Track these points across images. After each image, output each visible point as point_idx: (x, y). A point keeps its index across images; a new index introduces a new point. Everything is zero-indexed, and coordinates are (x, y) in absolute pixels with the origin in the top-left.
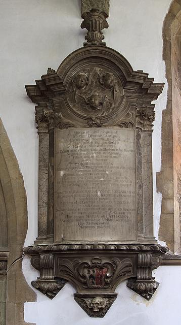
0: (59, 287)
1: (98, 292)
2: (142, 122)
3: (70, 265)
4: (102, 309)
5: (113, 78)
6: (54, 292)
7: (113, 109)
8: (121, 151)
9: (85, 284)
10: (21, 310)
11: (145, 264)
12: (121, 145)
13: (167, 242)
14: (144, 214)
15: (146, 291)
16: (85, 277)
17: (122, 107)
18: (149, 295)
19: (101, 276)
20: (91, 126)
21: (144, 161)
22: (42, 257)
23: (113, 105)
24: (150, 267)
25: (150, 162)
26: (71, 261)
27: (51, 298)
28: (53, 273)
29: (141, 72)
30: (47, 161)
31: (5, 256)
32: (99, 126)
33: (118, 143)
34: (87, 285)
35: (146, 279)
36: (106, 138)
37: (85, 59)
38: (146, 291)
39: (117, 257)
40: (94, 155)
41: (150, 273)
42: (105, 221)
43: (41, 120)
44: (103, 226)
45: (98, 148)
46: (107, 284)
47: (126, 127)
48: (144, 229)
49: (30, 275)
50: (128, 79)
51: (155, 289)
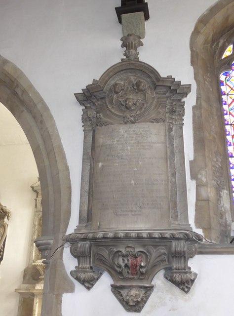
0: (96, 277)
1: (134, 284)
2: (173, 117)
3: (105, 253)
4: (138, 302)
5: (145, 84)
6: (91, 283)
7: (145, 109)
8: (153, 143)
9: (120, 273)
10: (59, 302)
11: (178, 253)
12: (153, 138)
13: (204, 229)
14: (178, 201)
15: (184, 284)
16: (120, 267)
17: (152, 108)
18: (187, 287)
19: (136, 266)
20: (126, 123)
21: (176, 151)
22: (79, 245)
23: (145, 105)
24: (183, 256)
25: (182, 151)
26: (106, 249)
27: (89, 288)
28: (90, 262)
29: (170, 77)
30: (90, 154)
31: (49, 244)
32: (133, 123)
33: (150, 136)
34: (123, 276)
35: (181, 269)
36: (139, 133)
37: (122, 70)
38: (184, 284)
39: (151, 245)
40: (129, 148)
41: (186, 261)
42: (138, 209)
43: (85, 119)
44: (136, 213)
45: (132, 142)
46: (142, 274)
47: (157, 123)
48: (179, 217)
49: (70, 263)
50: (157, 84)
51: (193, 281)
